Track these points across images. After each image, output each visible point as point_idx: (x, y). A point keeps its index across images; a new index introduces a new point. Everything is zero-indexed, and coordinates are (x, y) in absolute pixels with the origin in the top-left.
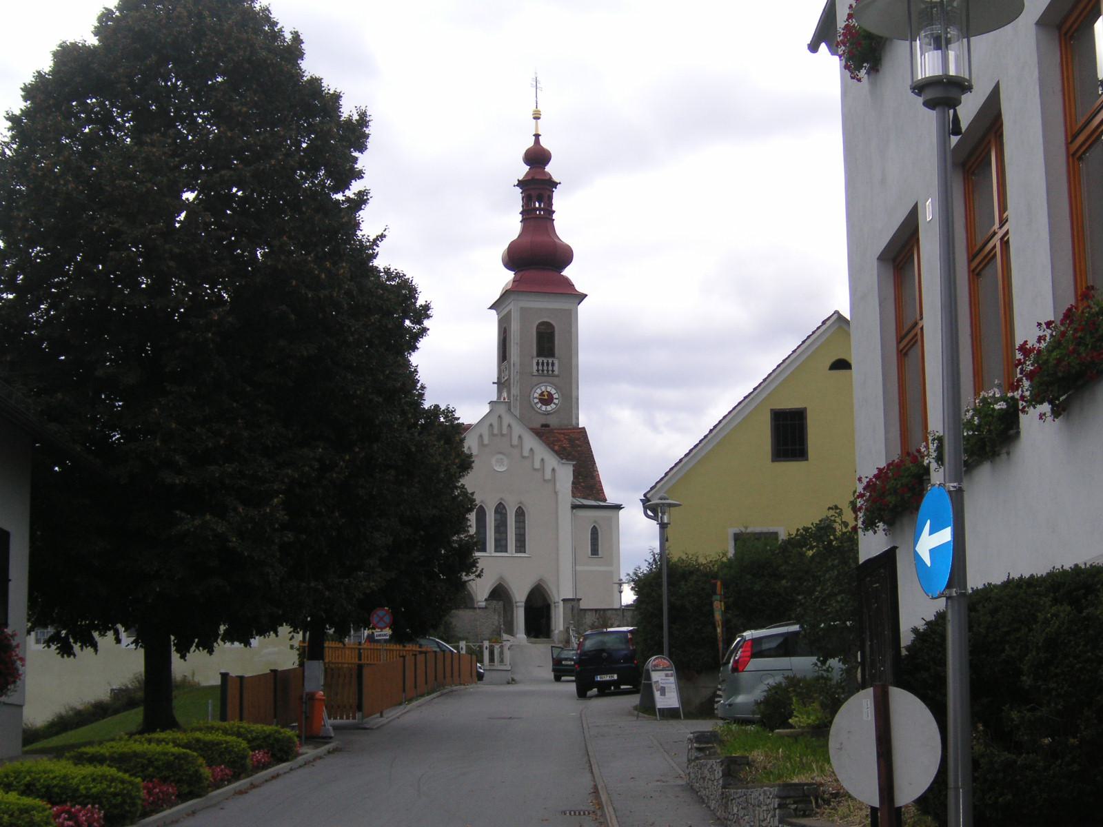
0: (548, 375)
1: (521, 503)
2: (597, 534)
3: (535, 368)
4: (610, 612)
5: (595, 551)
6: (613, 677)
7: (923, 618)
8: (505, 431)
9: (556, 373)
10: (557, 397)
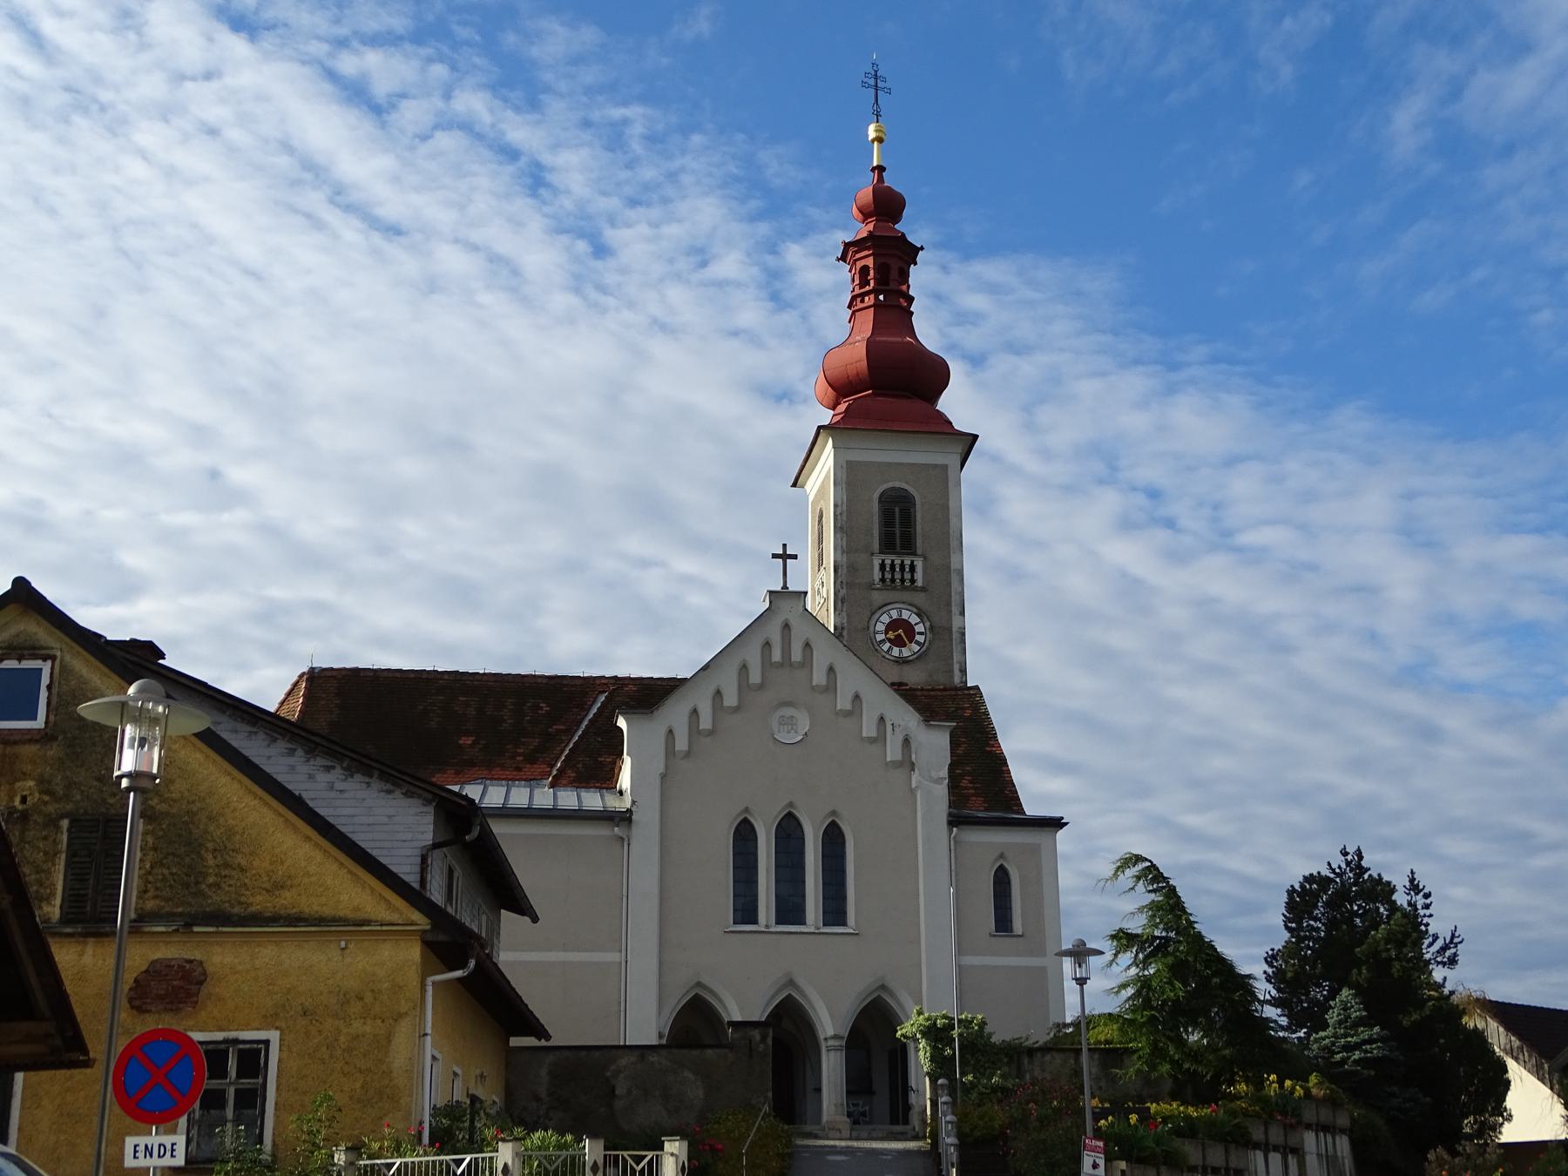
0: (905, 589)
1: (834, 813)
2: (1009, 883)
3: (877, 575)
5: (1003, 922)
7: (1445, 978)
8: (797, 655)
9: (919, 583)
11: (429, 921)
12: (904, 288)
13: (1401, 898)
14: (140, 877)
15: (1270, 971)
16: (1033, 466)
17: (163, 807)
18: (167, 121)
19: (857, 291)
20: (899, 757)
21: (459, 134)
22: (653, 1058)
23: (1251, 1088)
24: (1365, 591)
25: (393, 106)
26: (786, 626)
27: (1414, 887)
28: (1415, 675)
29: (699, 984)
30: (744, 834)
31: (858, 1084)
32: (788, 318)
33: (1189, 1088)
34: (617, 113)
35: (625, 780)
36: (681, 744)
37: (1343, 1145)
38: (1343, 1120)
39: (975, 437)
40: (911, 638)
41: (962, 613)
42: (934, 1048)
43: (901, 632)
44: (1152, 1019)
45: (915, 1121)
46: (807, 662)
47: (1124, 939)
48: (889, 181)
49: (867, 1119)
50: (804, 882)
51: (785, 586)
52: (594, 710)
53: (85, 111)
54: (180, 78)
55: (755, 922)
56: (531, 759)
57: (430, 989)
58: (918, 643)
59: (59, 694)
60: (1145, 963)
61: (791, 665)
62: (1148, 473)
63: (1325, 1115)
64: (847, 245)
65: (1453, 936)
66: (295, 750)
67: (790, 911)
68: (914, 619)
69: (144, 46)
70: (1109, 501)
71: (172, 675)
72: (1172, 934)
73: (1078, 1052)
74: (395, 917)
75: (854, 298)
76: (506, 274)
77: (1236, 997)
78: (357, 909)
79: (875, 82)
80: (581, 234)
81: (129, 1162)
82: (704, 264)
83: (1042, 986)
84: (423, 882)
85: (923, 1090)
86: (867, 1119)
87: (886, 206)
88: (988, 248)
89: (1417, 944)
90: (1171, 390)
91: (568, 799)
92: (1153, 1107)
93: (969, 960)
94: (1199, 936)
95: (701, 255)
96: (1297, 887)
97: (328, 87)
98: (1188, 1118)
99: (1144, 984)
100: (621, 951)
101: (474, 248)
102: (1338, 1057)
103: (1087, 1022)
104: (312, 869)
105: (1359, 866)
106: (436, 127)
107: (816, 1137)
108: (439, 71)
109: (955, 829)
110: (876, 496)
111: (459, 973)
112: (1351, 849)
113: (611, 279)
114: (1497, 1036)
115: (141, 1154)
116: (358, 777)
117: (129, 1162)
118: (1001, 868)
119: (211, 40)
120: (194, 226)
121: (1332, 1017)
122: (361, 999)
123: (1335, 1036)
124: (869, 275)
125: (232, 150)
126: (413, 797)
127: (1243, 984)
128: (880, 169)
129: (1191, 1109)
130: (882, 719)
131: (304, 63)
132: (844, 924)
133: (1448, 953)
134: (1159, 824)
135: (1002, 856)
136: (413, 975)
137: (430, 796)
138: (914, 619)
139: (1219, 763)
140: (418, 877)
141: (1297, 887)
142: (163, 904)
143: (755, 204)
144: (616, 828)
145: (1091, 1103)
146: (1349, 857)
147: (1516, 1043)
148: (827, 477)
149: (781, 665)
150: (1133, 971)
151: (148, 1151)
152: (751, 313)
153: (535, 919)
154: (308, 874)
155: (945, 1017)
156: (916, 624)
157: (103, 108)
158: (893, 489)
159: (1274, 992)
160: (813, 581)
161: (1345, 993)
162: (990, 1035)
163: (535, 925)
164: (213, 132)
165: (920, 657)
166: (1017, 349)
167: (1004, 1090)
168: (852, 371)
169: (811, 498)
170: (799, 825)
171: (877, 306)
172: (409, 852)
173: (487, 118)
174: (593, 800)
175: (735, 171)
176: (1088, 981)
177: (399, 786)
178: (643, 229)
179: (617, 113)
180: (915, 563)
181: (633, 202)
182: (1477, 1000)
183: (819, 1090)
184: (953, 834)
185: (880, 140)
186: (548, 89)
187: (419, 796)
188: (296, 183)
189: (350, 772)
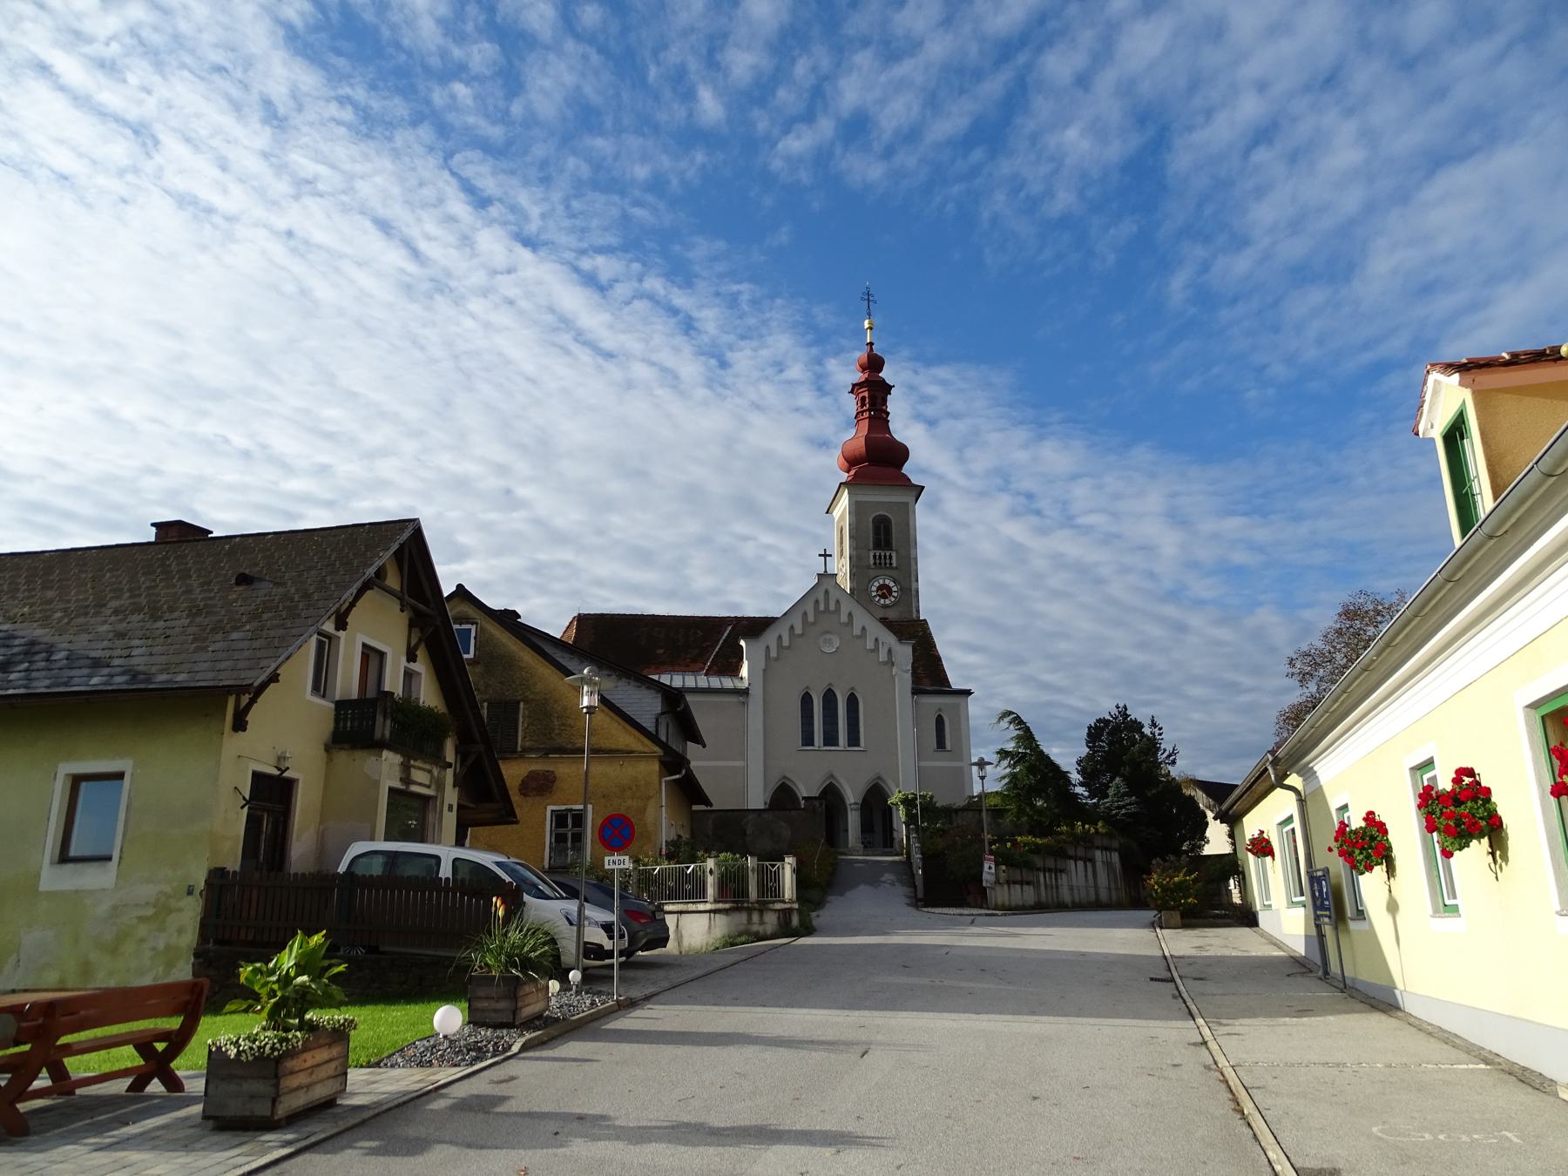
0: (887, 568)
3: (872, 561)
5: (941, 744)
6: (916, 854)
8: (832, 607)
9: (894, 565)
12: (884, 407)
13: (1147, 731)
14: (523, 730)
15: (1079, 768)
16: (962, 481)
17: (531, 696)
18: (485, 297)
19: (859, 410)
20: (886, 659)
21: (646, 301)
22: (765, 816)
23: (1069, 829)
24: (1147, 549)
25: (611, 286)
26: (827, 592)
27: (1154, 724)
28: (1174, 595)
29: (785, 777)
30: (807, 700)
31: (867, 827)
32: (828, 400)
33: (1037, 829)
34: (735, 288)
35: (744, 672)
36: (773, 654)
37: (1115, 857)
38: (1115, 844)
39: (923, 487)
40: (890, 594)
41: (917, 581)
42: (907, 810)
43: (885, 591)
44: (1018, 795)
45: (897, 846)
46: (838, 610)
47: (1003, 754)
50: (837, 724)
51: (826, 571)
52: (726, 635)
53: (442, 292)
54: (494, 272)
55: (813, 745)
56: (694, 661)
58: (894, 597)
59: (480, 642)
60: (1014, 766)
61: (830, 612)
62: (1027, 484)
63: (1106, 842)
64: (854, 386)
65: (1174, 750)
67: (831, 739)
68: (892, 584)
69: (474, 255)
70: (1004, 501)
71: (533, 631)
72: (1028, 751)
73: (981, 811)
74: (646, 750)
75: (858, 414)
76: (670, 377)
77: (1061, 782)
78: (628, 745)
79: (868, 297)
80: (713, 356)
81: (607, 867)
82: (781, 371)
83: (960, 777)
84: (657, 731)
85: (901, 831)
87: (874, 364)
88: (939, 360)
89: (1155, 754)
90: (1041, 438)
91: (715, 682)
92: (1019, 839)
93: (923, 764)
94: (1042, 752)
95: (780, 366)
96: (1093, 725)
97: (575, 276)
98: (1036, 844)
99: (1013, 776)
101: (653, 364)
102: (1114, 812)
103: (983, 796)
104: (605, 726)
105: (1125, 714)
106: (634, 297)
107: (846, 854)
108: (636, 266)
110: (871, 519)
111: (678, 776)
112: (1121, 705)
113: (729, 380)
114: (1202, 800)
115: (611, 864)
116: (624, 680)
117: (607, 867)
118: (940, 715)
119: (511, 251)
120: (500, 354)
121: (1111, 792)
122: (631, 789)
123: (1113, 802)
125: (521, 313)
127: (1064, 776)
128: (871, 344)
129: (1038, 839)
130: (877, 640)
131: (562, 264)
132: (858, 745)
133: (1171, 758)
134: (1028, 680)
135: (940, 710)
136: (655, 778)
138: (892, 584)
139: (1063, 645)
141: (1093, 725)
142: (534, 743)
143: (810, 337)
145: (988, 837)
146: (1120, 709)
147: (1212, 802)
148: (845, 509)
149: (824, 612)
150: (1008, 770)
151: (614, 862)
152: (806, 399)
153: (704, 746)
154: (603, 729)
155: (913, 794)
157: (451, 290)
158: (880, 515)
159: (1081, 779)
160: (838, 564)
161: (1117, 779)
162: (935, 803)
164: (511, 302)
165: (894, 604)
166: (956, 416)
167: (943, 830)
168: (857, 453)
169: (836, 520)
170: (835, 695)
171: (870, 417)
172: (650, 716)
173: (662, 292)
174: (728, 683)
175: (800, 319)
178: (748, 352)
179: (735, 288)
181: (743, 338)
182: (1191, 780)
183: (847, 831)
185: (871, 328)
186: (696, 276)
187: (654, 689)
188: (556, 330)
189: (620, 677)
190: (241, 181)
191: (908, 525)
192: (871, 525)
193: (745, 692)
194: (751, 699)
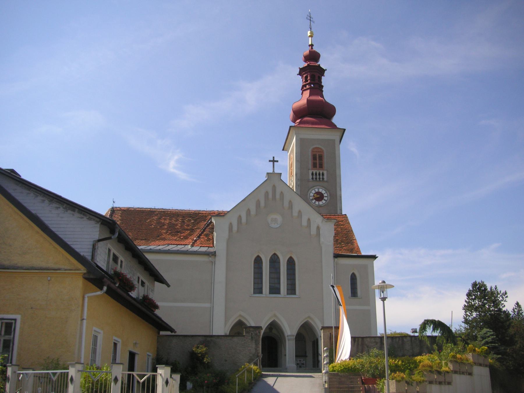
3: (311, 177)
4: (368, 339)
9: (325, 179)
10: (326, 195)
11: (86, 269)
19: (304, 83)
30: (258, 261)
39: (344, 130)
48: (315, 49)
49: (304, 366)
57: (86, 300)
58: (325, 200)
66: (45, 200)
79: (310, 18)
86: (304, 366)
100: (211, 303)
109: (336, 259)
110: (310, 150)
116: (69, 212)
124: (308, 78)
126: (91, 220)
128: (312, 45)
136: (78, 293)
137: (98, 220)
140: (91, 254)
144: (210, 258)
156: (324, 194)
163: (168, 288)
170: (278, 257)
176: (386, 299)
177: (86, 216)
180: (324, 173)
183: (285, 355)
184: (335, 261)
187: (94, 220)
190: (420, 382)
191: (335, 153)
192: (310, 154)
193: (214, 254)
194: (217, 258)
